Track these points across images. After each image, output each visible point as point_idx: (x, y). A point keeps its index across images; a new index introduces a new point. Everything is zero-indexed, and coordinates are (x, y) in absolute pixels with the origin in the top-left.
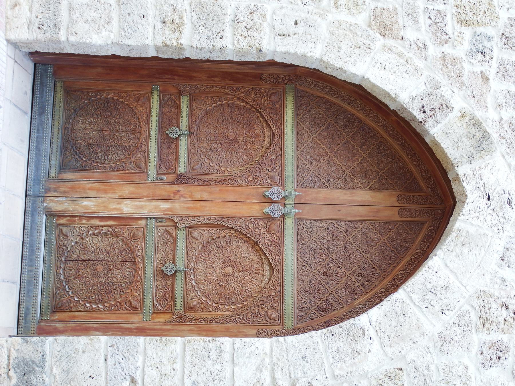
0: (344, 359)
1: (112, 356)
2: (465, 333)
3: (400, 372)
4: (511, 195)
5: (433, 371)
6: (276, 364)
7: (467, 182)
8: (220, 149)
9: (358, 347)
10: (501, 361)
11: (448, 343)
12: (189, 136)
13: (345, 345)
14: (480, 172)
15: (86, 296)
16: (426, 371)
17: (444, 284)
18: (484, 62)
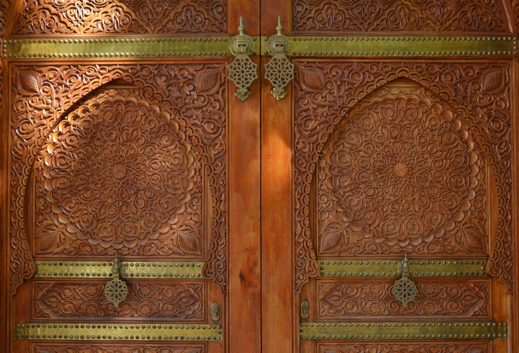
8: (148, 194)
12: (121, 260)
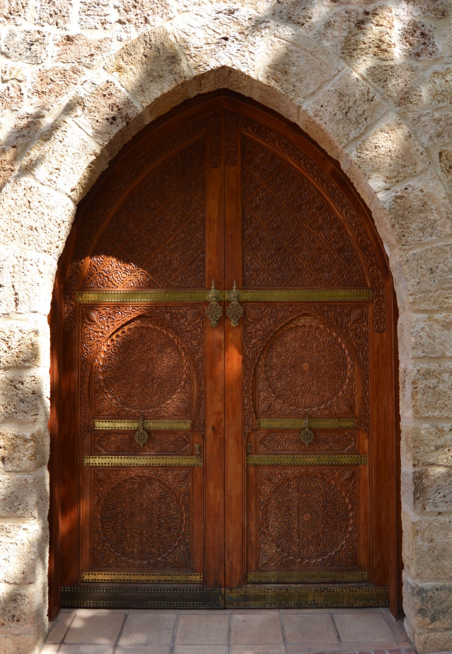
0: (433, 222)
1: (436, 506)
2: (394, 74)
3: (443, 154)
4: (220, 10)
5: (441, 115)
6: (441, 305)
7: (205, 65)
9: (416, 204)
10: (426, 32)
11: (407, 95)
13: (415, 220)
14: (192, 49)
15: (340, 531)
16: (441, 123)
17: (337, 98)
18: (45, 42)
